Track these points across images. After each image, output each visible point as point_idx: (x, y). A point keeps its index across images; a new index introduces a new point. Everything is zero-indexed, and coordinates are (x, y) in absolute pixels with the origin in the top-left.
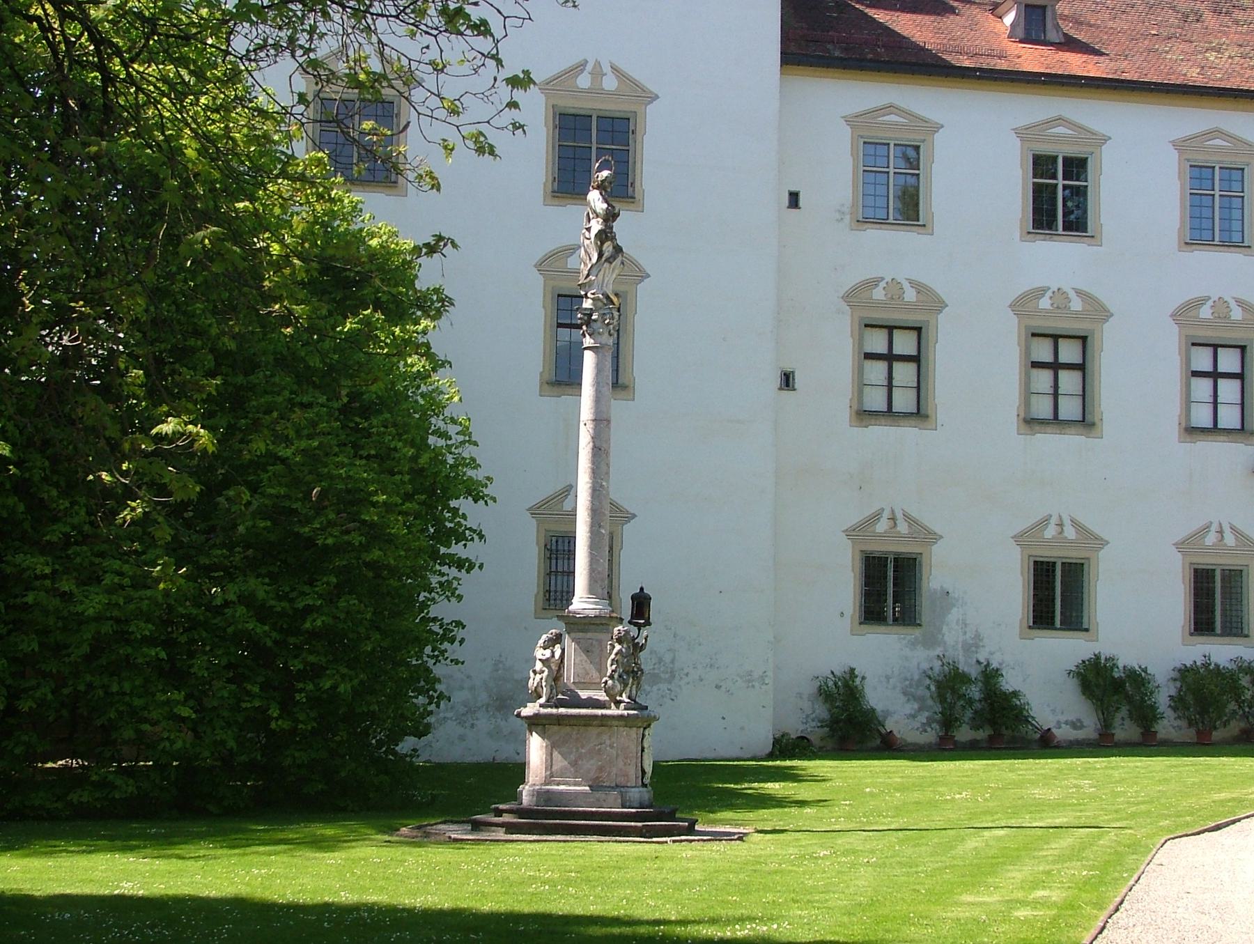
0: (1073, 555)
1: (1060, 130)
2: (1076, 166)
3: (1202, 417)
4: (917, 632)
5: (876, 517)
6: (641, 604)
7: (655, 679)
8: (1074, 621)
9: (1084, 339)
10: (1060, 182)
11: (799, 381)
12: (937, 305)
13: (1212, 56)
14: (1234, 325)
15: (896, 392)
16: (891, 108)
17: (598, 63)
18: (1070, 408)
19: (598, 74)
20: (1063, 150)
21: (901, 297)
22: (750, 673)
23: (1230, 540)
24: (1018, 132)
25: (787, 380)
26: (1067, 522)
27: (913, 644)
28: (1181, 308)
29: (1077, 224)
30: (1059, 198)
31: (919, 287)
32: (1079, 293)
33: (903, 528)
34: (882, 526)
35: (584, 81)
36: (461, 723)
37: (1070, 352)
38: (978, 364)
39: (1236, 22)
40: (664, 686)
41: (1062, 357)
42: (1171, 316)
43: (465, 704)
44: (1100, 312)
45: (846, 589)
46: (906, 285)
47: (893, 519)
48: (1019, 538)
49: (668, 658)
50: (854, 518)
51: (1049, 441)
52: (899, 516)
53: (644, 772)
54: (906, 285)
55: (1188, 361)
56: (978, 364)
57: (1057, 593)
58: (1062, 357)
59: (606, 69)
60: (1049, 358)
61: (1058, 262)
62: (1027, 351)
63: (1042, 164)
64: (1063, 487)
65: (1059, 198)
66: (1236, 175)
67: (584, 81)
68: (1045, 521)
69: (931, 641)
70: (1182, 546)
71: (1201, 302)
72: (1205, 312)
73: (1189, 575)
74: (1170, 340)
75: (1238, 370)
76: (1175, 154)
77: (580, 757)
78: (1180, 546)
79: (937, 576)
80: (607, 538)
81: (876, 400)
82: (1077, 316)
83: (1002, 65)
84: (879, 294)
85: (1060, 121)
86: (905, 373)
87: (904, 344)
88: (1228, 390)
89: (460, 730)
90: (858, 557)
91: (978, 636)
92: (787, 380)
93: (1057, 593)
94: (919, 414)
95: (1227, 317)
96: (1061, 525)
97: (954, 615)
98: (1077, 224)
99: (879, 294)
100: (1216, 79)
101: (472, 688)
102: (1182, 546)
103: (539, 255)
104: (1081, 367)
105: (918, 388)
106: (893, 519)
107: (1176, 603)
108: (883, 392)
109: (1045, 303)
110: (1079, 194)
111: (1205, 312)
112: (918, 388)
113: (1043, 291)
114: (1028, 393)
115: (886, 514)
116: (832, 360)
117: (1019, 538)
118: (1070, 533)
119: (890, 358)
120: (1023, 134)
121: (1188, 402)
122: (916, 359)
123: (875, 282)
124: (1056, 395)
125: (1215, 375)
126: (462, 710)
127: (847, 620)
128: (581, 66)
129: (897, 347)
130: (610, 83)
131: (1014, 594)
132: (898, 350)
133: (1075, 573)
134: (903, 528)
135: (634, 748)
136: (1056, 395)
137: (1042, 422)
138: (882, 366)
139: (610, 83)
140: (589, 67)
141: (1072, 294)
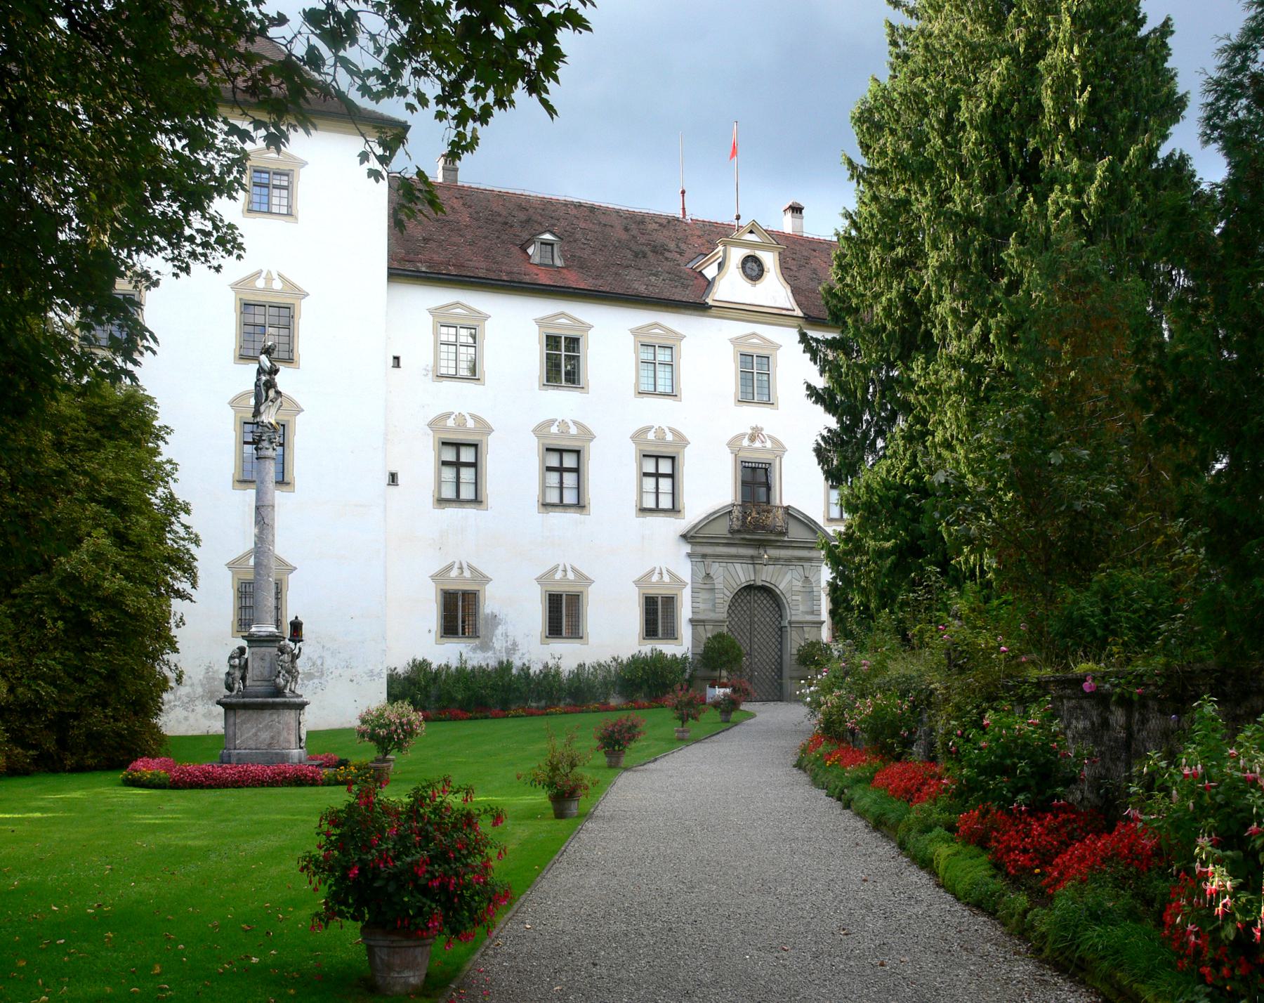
1: (563, 321)
2: (573, 342)
3: (649, 502)
4: (477, 641)
5: (450, 567)
6: (296, 627)
7: (310, 676)
8: (576, 633)
9: (673, 458)
10: (563, 353)
11: (400, 479)
12: (487, 429)
13: (653, 278)
14: (469, 431)
15: (661, 496)
16: (754, 335)
17: (269, 272)
18: (570, 497)
19: (269, 279)
20: (564, 333)
21: (464, 424)
22: (371, 671)
23: (666, 578)
24: (536, 321)
25: (393, 478)
26: (569, 569)
28: (539, 426)
29: (573, 378)
30: (563, 361)
32: (575, 423)
33: (467, 574)
34: (454, 573)
35: (260, 283)
36: (186, 709)
37: (665, 467)
38: (513, 468)
39: (667, 259)
40: (316, 681)
41: (565, 461)
42: (430, 425)
43: (188, 695)
44: (588, 435)
45: (432, 616)
46: (468, 417)
47: (461, 568)
48: (540, 580)
49: (319, 663)
50: (436, 568)
51: (452, 512)
52: (465, 566)
53: (300, 740)
54: (468, 417)
55: (641, 467)
56: (513, 468)
57: (563, 613)
58: (565, 461)
59: (275, 276)
60: (653, 470)
61: (562, 405)
62: (543, 460)
64: (568, 544)
65: (563, 361)
67: (260, 283)
68: (555, 569)
69: (485, 647)
73: (643, 601)
74: (630, 453)
75: (473, 460)
76: (431, 318)
77: (259, 730)
78: (637, 583)
79: (490, 603)
80: (273, 586)
81: (553, 497)
82: (574, 437)
83: (527, 279)
84: (450, 423)
85: (563, 315)
86: (569, 479)
87: (665, 467)
88: (665, 484)
89: (186, 714)
90: (439, 593)
91: (515, 644)
92: (393, 478)
93: (563, 613)
94: (477, 501)
95: (664, 439)
96: (565, 571)
97: (500, 630)
98: (573, 378)
99: (450, 423)
100: (655, 292)
101: (192, 685)
103: (232, 396)
105: (476, 483)
106: (461, 568)
107: (635, 618)
108: (653, 497)
109: (554, 429)
110: (574, 360)
112: (476, 483)
113: (553, 421)
114: (544, 488)
115: (457, 566)
116: (421, 465)
117: (540, 580)
118: (571, 576)
119: (657, 475)
120: (540, 322)
121: (641, 492)
122: (474, 465)
123: (448, 415)
124: (657, 493)
125: (657, 475)
126: (186, 700)
127: (433, 633)
128: (259, 274)
129: (461, 456)
130: (277, 285)
132: (565, 465)
133: (575, 600)
134: (467, 574)
135: (294, 724)
137: (553, 505)
138: (652, 481)
139: (277, 285)
140: (264, 275)
141: (571, 424)
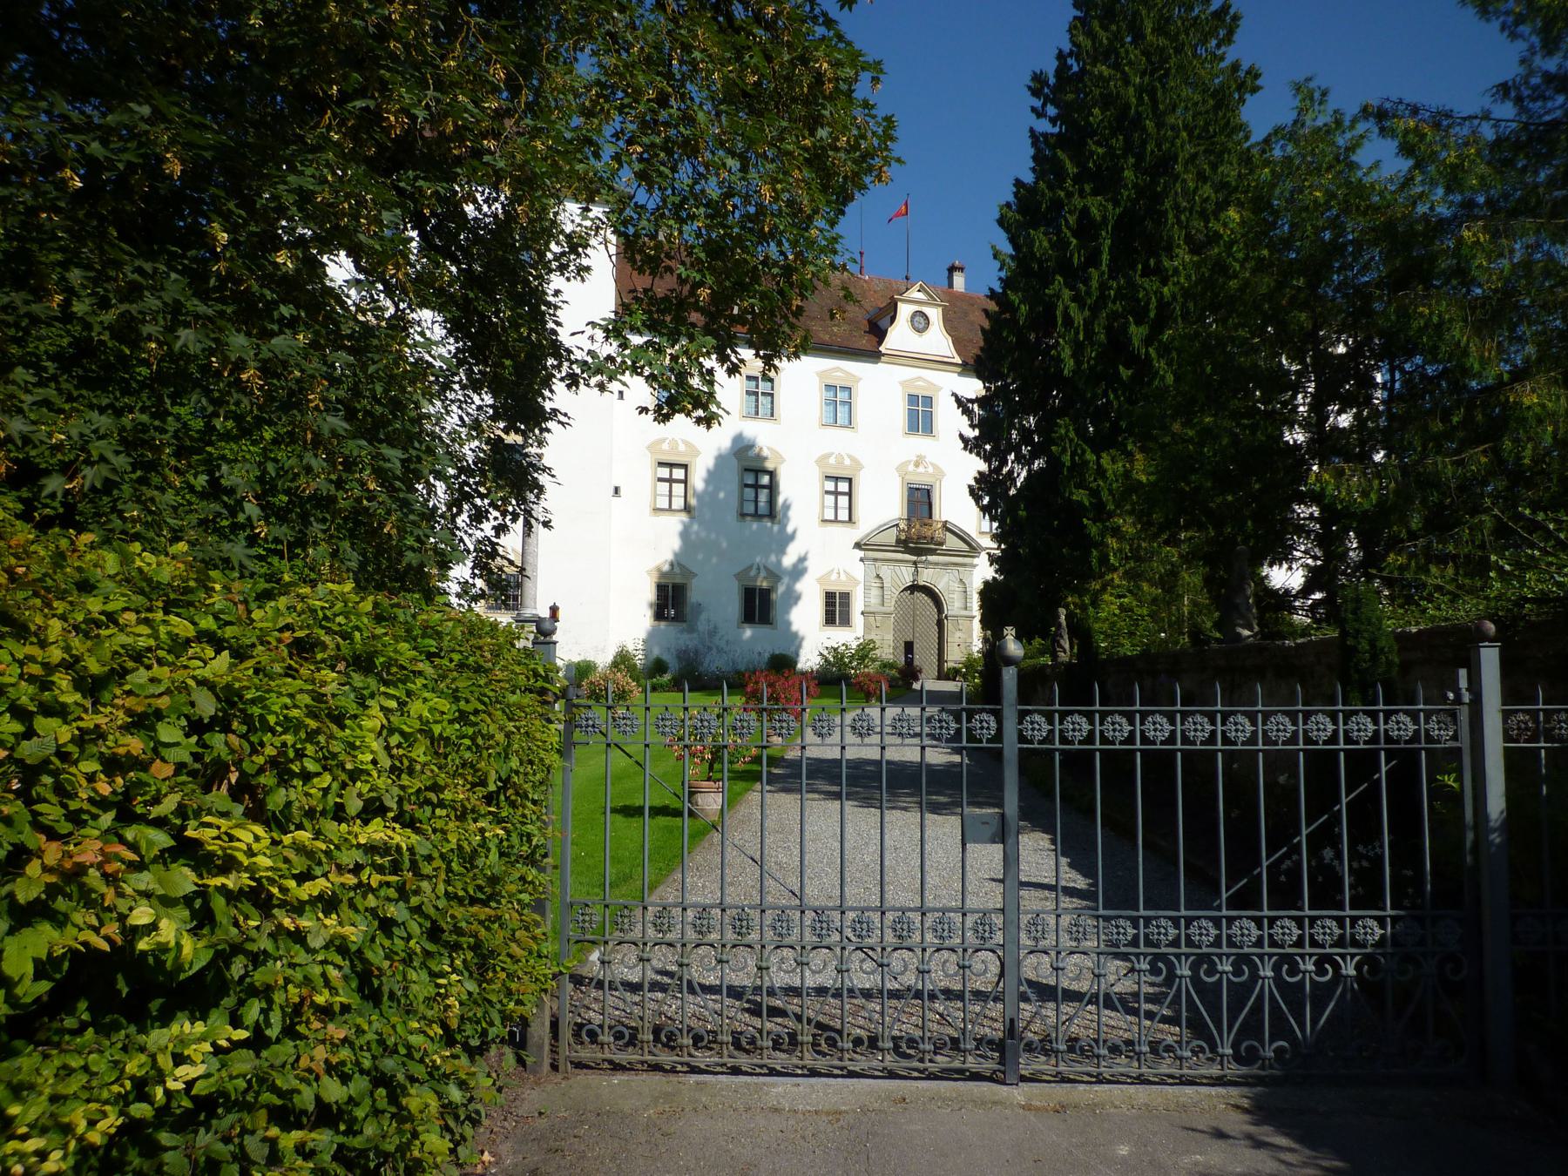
0: (844, 589)
2: (929, 401)
3: (830, 515)
11: (622, 492)
16: (919, 378)
20: (921, 393)
27: (682, 631)
31: (686, 443)
34: (834, 577)
42: (648, 448)
63: (913, 399)
66: (842, 396)
70: (738, 576)
71: (830, 455)
72: (665, 446)
74: (815, 475)
79: (694, 595)
97: (703, 617)
102: (738, 576)
104: (850, 494)
111: (832, 460)
118: (843, 577)
124: (670, 496)
131: (732, 606)
136: (670, 496)
138: (832, 498)
